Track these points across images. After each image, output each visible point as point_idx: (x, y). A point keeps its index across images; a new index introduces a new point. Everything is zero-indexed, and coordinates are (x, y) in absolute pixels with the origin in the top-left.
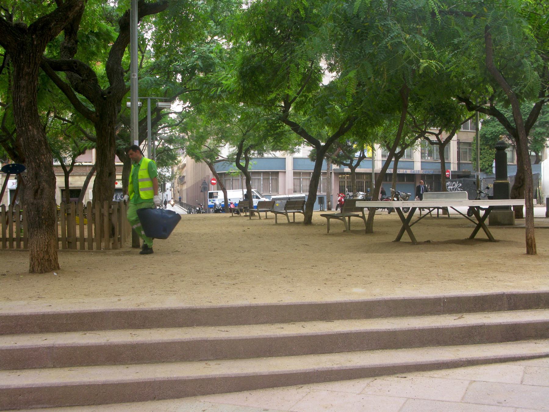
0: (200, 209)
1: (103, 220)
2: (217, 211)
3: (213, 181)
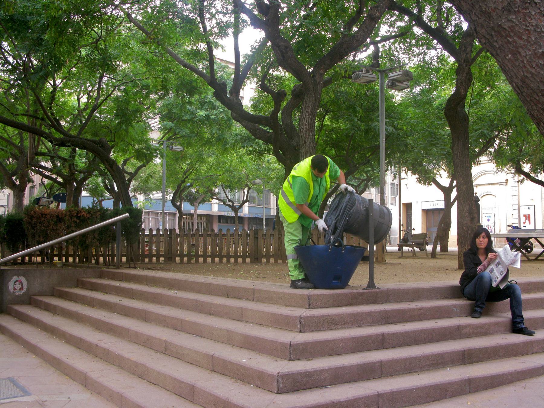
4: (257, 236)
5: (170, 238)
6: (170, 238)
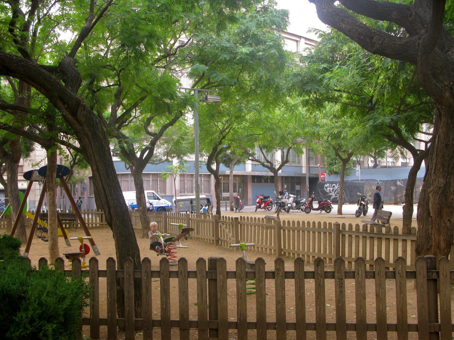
4: (434, 276)
5: (213, 281)
6: (213, 281)
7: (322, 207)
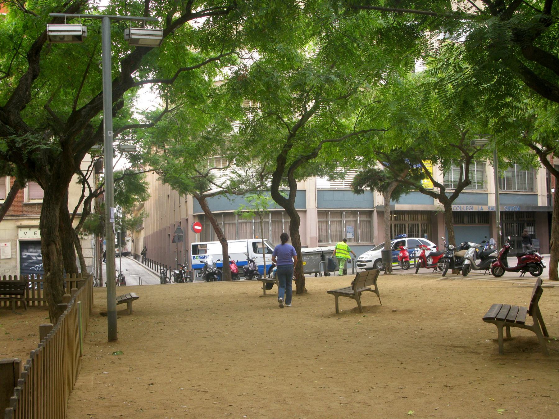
0: (181, 272)
1: (81, 264)
2: (210, 277)
3: (196, 227)
7: (523, 267)
